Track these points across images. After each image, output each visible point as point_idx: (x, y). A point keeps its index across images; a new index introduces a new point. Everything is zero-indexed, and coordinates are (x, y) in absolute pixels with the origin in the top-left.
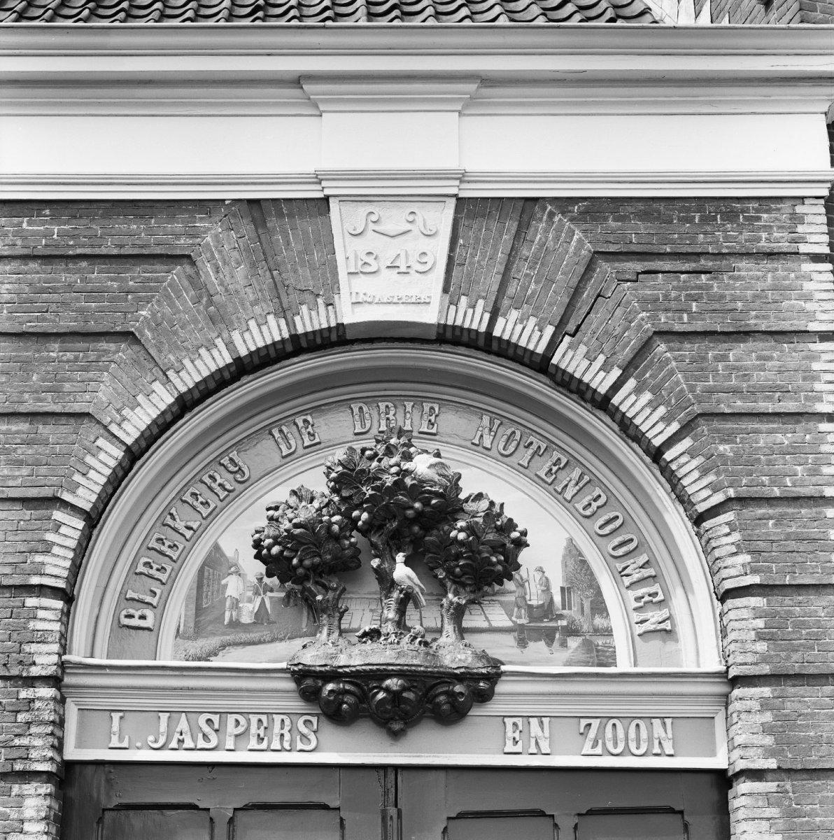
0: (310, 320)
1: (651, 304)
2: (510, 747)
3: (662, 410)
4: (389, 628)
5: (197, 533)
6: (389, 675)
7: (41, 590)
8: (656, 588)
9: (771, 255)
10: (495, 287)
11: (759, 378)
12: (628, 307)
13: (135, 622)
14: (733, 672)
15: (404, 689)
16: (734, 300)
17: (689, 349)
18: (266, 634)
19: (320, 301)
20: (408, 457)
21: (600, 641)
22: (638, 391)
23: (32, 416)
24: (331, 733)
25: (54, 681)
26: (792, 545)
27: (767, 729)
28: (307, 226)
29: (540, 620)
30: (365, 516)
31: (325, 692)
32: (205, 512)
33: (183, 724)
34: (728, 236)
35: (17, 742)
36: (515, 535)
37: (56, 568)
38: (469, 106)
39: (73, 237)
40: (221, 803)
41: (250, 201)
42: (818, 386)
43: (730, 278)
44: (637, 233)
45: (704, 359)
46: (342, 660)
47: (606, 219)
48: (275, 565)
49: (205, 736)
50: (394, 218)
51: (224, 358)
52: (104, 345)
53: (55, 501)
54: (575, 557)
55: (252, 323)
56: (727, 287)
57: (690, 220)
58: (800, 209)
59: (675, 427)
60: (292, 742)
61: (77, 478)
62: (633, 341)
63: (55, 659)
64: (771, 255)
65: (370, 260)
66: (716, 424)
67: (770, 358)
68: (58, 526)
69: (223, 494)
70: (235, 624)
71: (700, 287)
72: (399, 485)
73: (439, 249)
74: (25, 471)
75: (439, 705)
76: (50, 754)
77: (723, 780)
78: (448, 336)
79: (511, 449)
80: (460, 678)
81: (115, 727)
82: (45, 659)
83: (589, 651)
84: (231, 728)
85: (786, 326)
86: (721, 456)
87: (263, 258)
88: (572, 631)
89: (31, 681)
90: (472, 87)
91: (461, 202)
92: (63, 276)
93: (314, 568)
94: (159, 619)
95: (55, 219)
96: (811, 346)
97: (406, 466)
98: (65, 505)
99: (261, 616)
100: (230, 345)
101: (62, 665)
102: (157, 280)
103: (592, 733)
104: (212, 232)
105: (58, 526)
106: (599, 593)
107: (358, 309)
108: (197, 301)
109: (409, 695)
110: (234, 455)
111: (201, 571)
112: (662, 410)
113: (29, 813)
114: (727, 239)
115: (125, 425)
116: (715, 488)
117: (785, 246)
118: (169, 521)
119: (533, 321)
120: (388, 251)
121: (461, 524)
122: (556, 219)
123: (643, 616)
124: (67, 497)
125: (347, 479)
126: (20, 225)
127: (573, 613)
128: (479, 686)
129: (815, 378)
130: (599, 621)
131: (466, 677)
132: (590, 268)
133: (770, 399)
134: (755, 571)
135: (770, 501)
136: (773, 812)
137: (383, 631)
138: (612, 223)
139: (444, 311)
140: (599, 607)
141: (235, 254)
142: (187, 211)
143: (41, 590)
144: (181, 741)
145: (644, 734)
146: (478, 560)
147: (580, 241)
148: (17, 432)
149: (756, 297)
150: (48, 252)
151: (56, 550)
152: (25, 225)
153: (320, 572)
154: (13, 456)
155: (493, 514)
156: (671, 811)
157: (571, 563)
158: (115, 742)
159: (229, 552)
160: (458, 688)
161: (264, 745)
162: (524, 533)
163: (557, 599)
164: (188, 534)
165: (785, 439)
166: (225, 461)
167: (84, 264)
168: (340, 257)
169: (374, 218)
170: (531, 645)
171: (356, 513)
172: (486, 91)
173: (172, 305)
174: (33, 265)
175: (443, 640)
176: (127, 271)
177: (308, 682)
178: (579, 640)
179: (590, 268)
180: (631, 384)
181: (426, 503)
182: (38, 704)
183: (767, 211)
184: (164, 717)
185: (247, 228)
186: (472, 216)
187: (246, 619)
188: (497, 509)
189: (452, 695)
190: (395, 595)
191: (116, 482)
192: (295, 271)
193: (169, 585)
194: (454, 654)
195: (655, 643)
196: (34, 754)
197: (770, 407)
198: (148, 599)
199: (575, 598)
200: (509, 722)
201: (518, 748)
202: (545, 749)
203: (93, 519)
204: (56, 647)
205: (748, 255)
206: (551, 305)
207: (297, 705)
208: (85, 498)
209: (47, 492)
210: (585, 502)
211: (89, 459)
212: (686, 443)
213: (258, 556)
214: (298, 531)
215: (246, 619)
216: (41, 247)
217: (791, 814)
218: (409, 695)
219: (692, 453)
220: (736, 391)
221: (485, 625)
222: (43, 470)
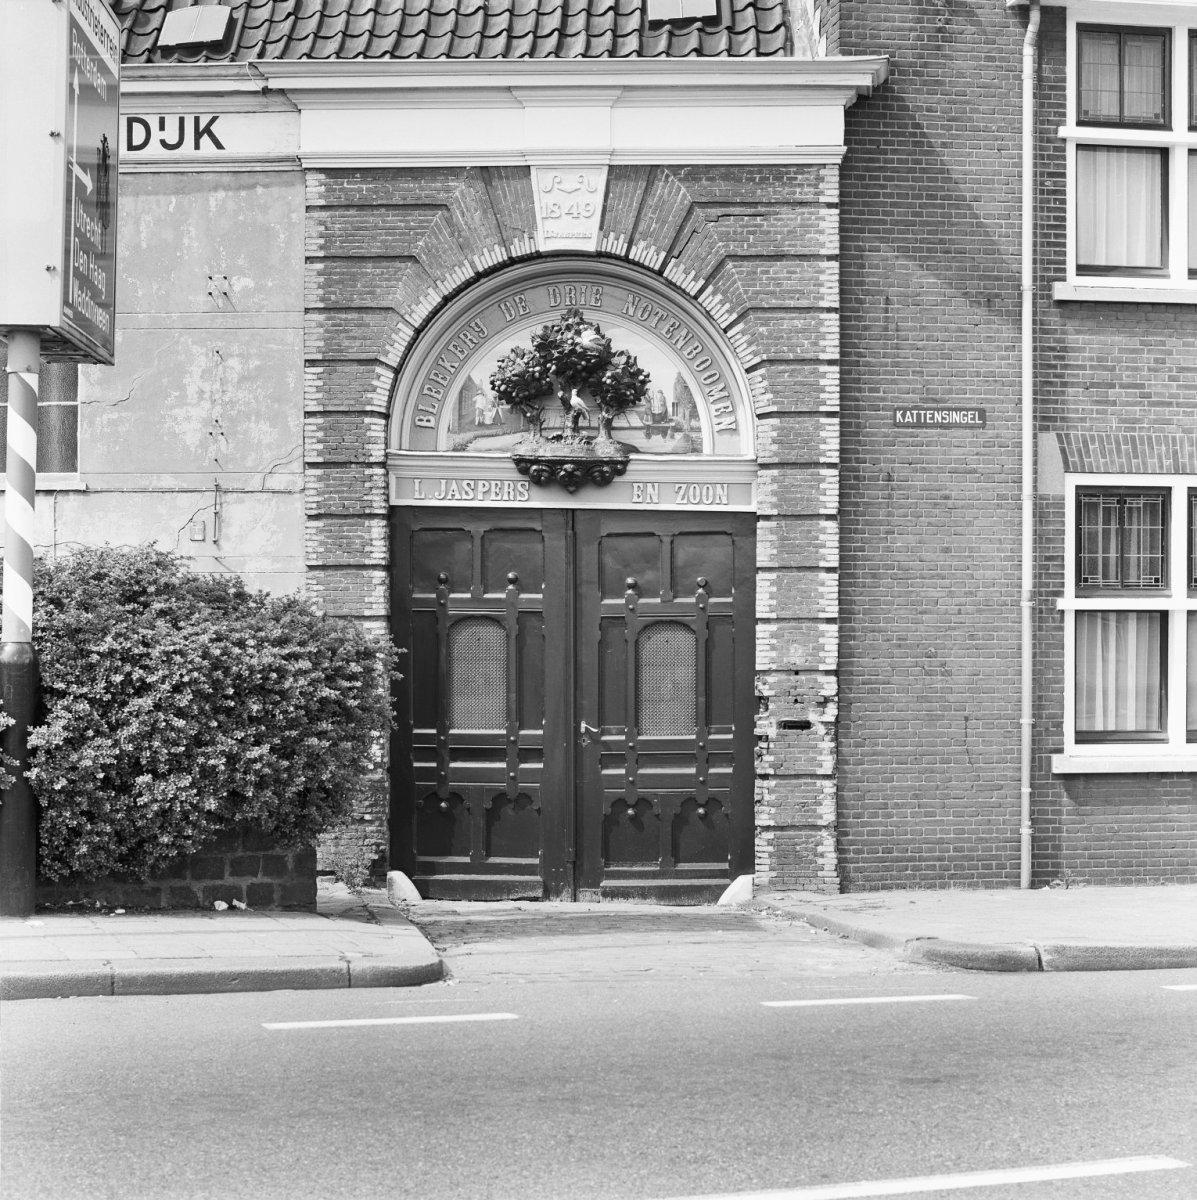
0: (519, 249)
1: (725, 237)
2: (635, 499)
3: (727, 306)
4: (568, 432)
5: (458, 370)
6: (567, 462)
7: (372, 413)
8: (728, 403)
9: (802, 204)
10: (631, 226)
11: (787, 285)
12: (714, 236)
13: (424, 424)
14: (760, 461)
15: (574, 470)
16: (776, 233)
17: (747, 266)
18: (500, 431)
19: (526, 235)
20: (578, 333)
21: (694, 435)
22: (714, 293)
23: (360, 309)
24: (536, 491)
25: (383, 465)
26: (798, 388)
27: (774, 493)
28: (517, 184)
29: (659, 422)
30: (554, 367)
31: (532, 471)
32: (462, 357)
33: (454, 486)
34: (774, 191)
35: (365, 498)
36: (641, 378)
37: (379, 401)
38: (616, 103)
39: (376, 193)
40: (478, 528)
41: (481, 167)
42: (823, 290)
43: (775, 219)
44: (720, 189)
45: (755, 273)
46: (541, 453)
47: (701, 179)
48: (504, 396)
49: (467, 493)
50: (570, 180)
51: (469, 273)
52: (398, 264)
53: (375, 361)
54: (680, 380)
55: (485, 250)
56: (772, 226)
57: (753, 180)
58: (822, 172)
59: (735, 316)
60: (515, 496)
61: (388, 347)
62: (713, 261)
63: (383, 452)
64: (802, 204)
65: (555, 209)
66: (760, 315)
67: (795, 272)
68: (379, 377)
69: (472, 346)
70: (481, 425)
71: (756, 226)
72: (573, 352)
73: (598, 200)
74: (358, 343)
75: (595, 477)
76: (384, 504)
77: (754, 517)
78: (600, 255)
79: (646, 316)
80: (607, 463)
81: (417, 488)
82: (377, 453)
83: (687, 441)
84: (480, 488)
85: (806, 251)
86: (761, 334)
87: (491, 206)
88: (677, 429)
89: (370, 465)
90: (618, 92)
91: (610, 166)
92: (371, 219)
93: (525, 397)
94: (438, 422)
95: (364, 181)
96: (820, 263)
97: (578, 340)
98: (382, 363)
99: (496, 420)
100: (472, 264)
101: (386, 455)
102: (427, 221)
103: (682, 492)
104: (459, 187)
105: (379, 377)
106: (695, 407)
107: (548, 241)
108: (452, 234)
109: (578, 473)
110: (478, 321)
111: (461, 393)
112: (727, 306)
113: (375, 536)
114: (775, 192)
115: (413, 315)
116: (755, 354)
117: (810, 197)
118: (440, 362)
119: (653, 248)
120: (567, 202)
121: (609, 374)
122: (670, 179)
123: (719, 421)
124: (383, 359)
125: (545, 345)
126: (342, 184)
127: (679, 418)
128: (618, 468)
129: (821, 285)
130: (694, 423)
131: (611, 463)
132: (690, 212)
133: (792, 298)
134: (774, 403)
135: (787, 362)
136: (774, 537)
137: (565, 435)
138: (704, 182)
139: (600, 242)
140: (694, 414)
141: (474, 203)
142: (444, 174)
143: (372, 413)
144: (453, 495)
145: (711, 492)
146: (622, 390)
147: (684, 195)
148: (353, 319)
149: (789, 232)
150: (361, 203)
151: (378, 390)
152: (345, 185)
153: (528, 400)
154: (351, 334)
155: (630, 362)
156: (726, 533)
157: (679, 388)
158: (417, 496)
159: (477, 381)
160: (606, 469)
161: (499, 498)
162: (648, 376)
163: (670, 409)
164: (453, 370)
165: (799, 324)
166: (473, 324)
167: (383, 210)
168: (537, 209)
169: (557, 180)
170: (654, 437)
171: (549, 365)
172: (626, 94)
173: (437, 238)
174: (352, 212)
175: (599, 439)
176: (410, 215)
177: (522, 464)
178: (681, 434)
179: (690, 212)
180: (710, 289)
181: (588, 361)
182: (375, 478)
183: (802, 174)
184: (443, 482)
185: (480, 185)
186: (618, 178)
187: (488, 421)
188: (632, 361)
189: (602, 473)
190: (572, 413)
191: (410, 347)
192: (510, 215)
193: (442, 402)
194: (604, 448)
195: (726, 436)
196: (375, 505)
197: (792, 303)
198: (431, 410)
199: (680, 410)
200: (635, 485)
201: (640, 500)
202: (655, 500)
203: (397, 371)
204: (383, 446)
205: (788, 203)
206: (664, 238)
207: (517, 476)
208: (393, 360)
209: (371, 356)
210: (689, 350)
211: (394, 336)
212: (740, 327)
213: (493, 389)
214: (515, 378)
215: (488, 421)
216: (356, 199)
217: (783, 539)
218: (578, 473)
219: (743, 332)
220: (773, 293)
221: (626, 425)
222: (368, 342)
